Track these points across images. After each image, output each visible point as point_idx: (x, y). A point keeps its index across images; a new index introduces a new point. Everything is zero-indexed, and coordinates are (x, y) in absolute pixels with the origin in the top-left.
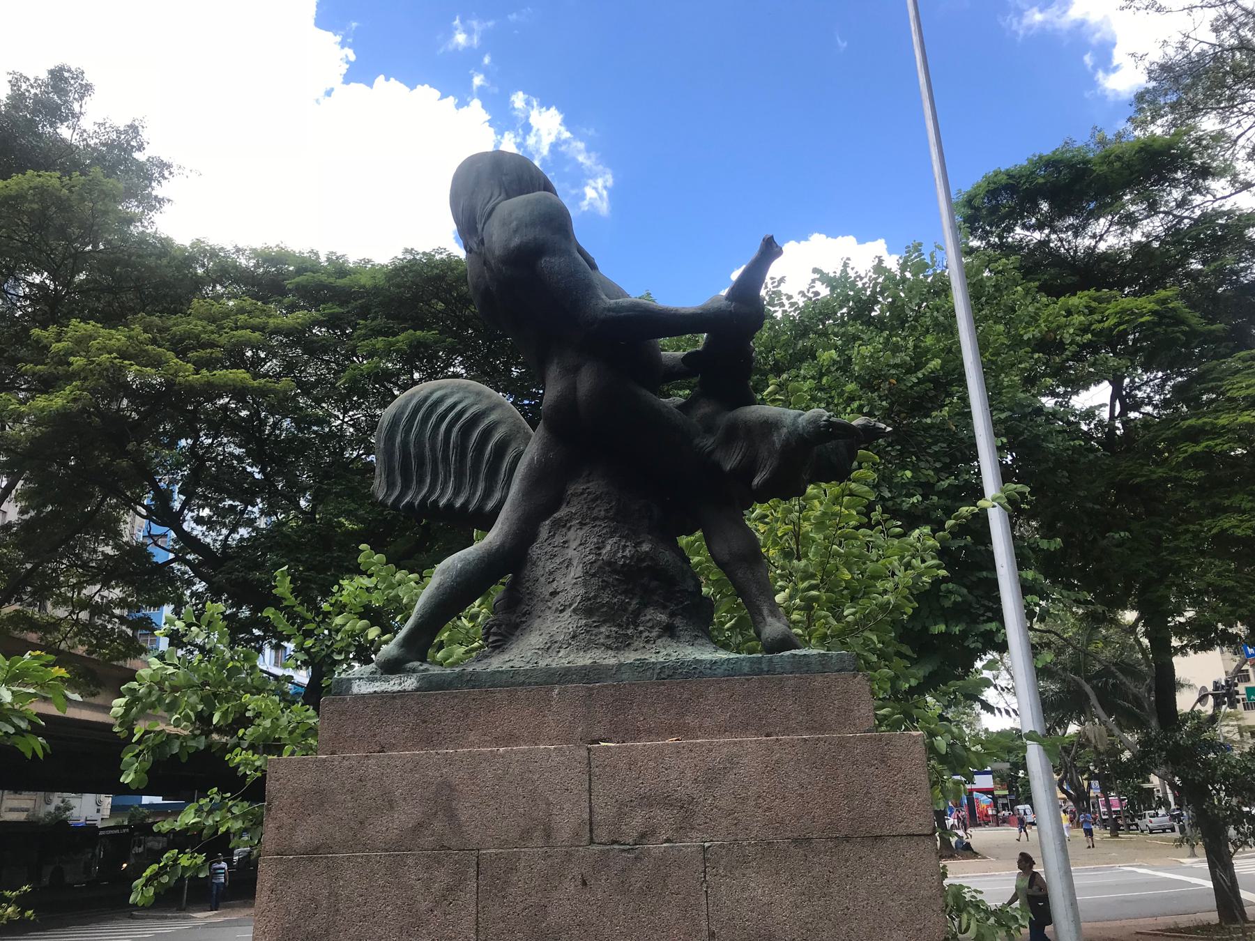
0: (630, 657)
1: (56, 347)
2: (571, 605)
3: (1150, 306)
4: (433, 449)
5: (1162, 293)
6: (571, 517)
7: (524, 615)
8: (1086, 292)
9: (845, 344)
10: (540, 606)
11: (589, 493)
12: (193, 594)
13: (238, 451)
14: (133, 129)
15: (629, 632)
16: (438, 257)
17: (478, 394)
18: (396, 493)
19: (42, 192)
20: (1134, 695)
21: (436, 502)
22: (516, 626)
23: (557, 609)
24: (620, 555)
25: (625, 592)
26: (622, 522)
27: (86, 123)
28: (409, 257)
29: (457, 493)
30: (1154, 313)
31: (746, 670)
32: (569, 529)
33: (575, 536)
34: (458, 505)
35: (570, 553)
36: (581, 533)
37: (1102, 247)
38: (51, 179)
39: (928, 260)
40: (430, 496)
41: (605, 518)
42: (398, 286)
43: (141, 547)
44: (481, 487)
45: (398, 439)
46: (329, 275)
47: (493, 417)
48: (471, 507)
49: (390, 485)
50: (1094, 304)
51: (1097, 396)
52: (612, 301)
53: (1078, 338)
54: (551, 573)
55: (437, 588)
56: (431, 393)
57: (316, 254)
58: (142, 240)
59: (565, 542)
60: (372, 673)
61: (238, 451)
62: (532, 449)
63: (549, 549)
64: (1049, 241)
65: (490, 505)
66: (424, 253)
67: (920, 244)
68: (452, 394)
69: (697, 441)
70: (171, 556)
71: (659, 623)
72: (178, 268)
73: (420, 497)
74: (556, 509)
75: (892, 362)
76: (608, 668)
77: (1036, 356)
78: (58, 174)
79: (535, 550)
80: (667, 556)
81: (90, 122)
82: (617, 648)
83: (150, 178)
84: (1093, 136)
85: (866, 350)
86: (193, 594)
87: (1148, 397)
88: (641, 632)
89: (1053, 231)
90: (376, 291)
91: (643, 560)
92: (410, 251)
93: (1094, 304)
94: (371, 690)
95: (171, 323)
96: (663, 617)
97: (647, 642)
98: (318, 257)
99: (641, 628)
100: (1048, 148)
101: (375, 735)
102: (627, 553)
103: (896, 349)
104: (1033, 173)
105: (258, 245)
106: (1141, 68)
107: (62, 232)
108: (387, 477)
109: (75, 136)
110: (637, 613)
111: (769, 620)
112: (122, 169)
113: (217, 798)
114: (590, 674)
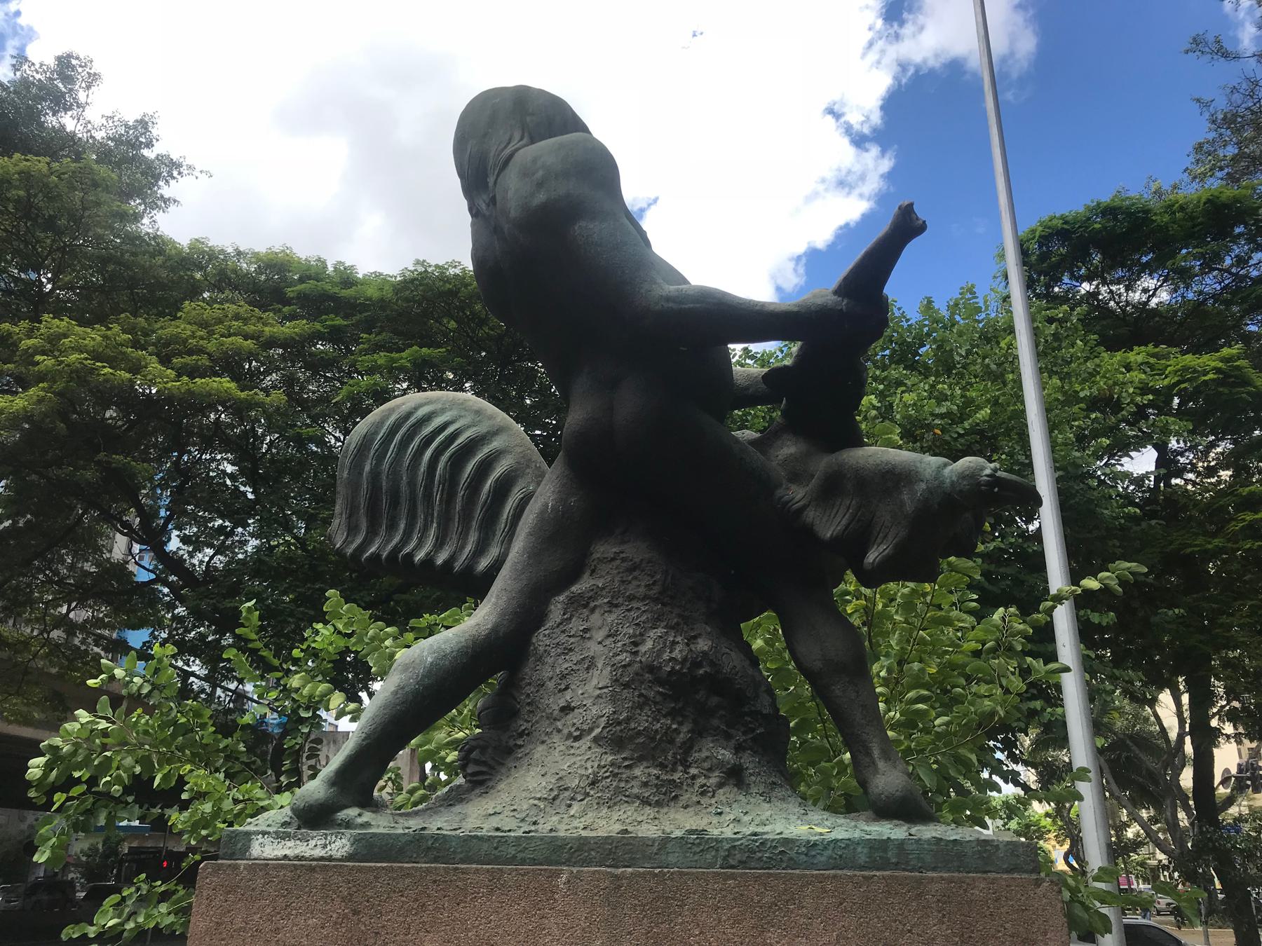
0: (679, 822)
1: (27, 343)
2: (591, 730)
3: (1213, 364)
4: (412, 483)
5: (1226, 351)
6: (596, 593)
7: (521, 735)
8: (1143, 348)
9: (888, 387)
10: (545, 726)
11: (624, 560)
12: (174, 618)
13: (230, 469)
14: (143, 124)
15: (676, 776)
16: (452, 271)
17: (478, 412)
18: (359, 540)
19: (26, 176)
20: (1148, 770)
21: (410, 556)
22: (509, 751)
23: (570, 735)
24: (666, 656)
25: (672, 714)
26: (669, 603)
27: (94, 114)
28: (421, 269)
29: (439, 544)
30: (1218, 370)
31: (863, 859)
32: (593, 610)
33: (600, 621)
34: (439, 561)
35: (593, 648)
36: (610, 618)
37: (1154, 302)
38: (39, 164)
39: (981, 304)
40: (404, 546)
41: (645, 597)
42: (407, 300)
43: (122, 566)
44: (473, 538)
45: (367, 468)
46: (334, 284)
47: (496, 444)
48: (458, 566)
49: (352, 530)
50: (1152, 360)
51: (1143, 462)
52: (672, 288)
53: (1138, 399)
54: (563, 677)
55: (395, 693)
56: (416, 409)
57: (324, 263)
58: (135, 239)
59: (586, 630)
60: (285, 824)
61: (230, 469)
62: (544, 492)
63: (563, 638)
64: (1099, 293)
65: (483, 564)
66: (437, 266)
67: (973, 286)
68: (443, 411)
69: (779, 492)
70: (153, 576)
71: (721, 764)
72: (173, 269)
73: (389, 547)
74: (574, 577)
75: (937, 411)
76: (646, 843)
77: (1093, 416)
78: (48, 159)
79: (542, 639)
80: (732, 661)
81: (94, 116)
82: (658, 804)
83: (157, 177)
84: (1148, 187)
85: (909, 398)
86: (174, 618)
87: (1191, 463)
88: (694, 777)
89: (1104, 283)
90: (382, 303)
91: (699, 665)
92: (422, 263)
93: (1152, 360)
94: (280, 853)
95: (158, 325)
96: (725, 755)
97: (703, 794)
98: (325, 267)
99: (693, 771)
100: (1106, 197)
101: (277, 931)
102: (676, 654)
103: (942, 398)
104: (1089, 219)
105: (261, 248)
106: (1207, 115)
107: (50, 224)
108: (350, 517)
109: (79, 127)
110: (688, 747)
111: (881, 765)
112: (131, 167)
113: (145, 887)
114: (618, 851)
